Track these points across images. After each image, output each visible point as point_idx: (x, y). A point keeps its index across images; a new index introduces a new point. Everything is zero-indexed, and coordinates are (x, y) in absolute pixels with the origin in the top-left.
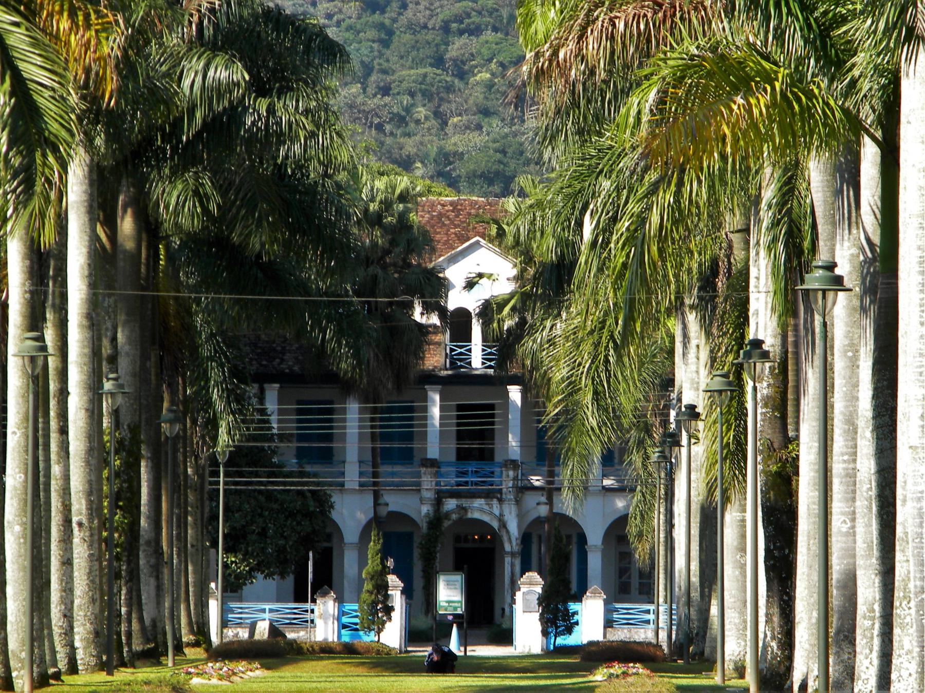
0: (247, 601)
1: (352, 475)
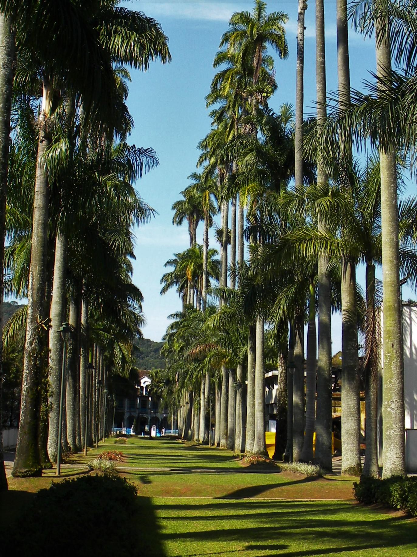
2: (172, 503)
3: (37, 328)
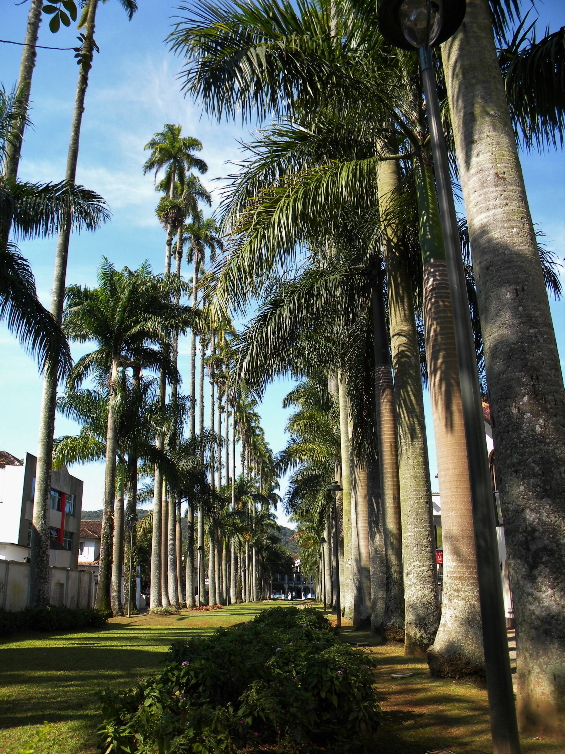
1: (286, 582)
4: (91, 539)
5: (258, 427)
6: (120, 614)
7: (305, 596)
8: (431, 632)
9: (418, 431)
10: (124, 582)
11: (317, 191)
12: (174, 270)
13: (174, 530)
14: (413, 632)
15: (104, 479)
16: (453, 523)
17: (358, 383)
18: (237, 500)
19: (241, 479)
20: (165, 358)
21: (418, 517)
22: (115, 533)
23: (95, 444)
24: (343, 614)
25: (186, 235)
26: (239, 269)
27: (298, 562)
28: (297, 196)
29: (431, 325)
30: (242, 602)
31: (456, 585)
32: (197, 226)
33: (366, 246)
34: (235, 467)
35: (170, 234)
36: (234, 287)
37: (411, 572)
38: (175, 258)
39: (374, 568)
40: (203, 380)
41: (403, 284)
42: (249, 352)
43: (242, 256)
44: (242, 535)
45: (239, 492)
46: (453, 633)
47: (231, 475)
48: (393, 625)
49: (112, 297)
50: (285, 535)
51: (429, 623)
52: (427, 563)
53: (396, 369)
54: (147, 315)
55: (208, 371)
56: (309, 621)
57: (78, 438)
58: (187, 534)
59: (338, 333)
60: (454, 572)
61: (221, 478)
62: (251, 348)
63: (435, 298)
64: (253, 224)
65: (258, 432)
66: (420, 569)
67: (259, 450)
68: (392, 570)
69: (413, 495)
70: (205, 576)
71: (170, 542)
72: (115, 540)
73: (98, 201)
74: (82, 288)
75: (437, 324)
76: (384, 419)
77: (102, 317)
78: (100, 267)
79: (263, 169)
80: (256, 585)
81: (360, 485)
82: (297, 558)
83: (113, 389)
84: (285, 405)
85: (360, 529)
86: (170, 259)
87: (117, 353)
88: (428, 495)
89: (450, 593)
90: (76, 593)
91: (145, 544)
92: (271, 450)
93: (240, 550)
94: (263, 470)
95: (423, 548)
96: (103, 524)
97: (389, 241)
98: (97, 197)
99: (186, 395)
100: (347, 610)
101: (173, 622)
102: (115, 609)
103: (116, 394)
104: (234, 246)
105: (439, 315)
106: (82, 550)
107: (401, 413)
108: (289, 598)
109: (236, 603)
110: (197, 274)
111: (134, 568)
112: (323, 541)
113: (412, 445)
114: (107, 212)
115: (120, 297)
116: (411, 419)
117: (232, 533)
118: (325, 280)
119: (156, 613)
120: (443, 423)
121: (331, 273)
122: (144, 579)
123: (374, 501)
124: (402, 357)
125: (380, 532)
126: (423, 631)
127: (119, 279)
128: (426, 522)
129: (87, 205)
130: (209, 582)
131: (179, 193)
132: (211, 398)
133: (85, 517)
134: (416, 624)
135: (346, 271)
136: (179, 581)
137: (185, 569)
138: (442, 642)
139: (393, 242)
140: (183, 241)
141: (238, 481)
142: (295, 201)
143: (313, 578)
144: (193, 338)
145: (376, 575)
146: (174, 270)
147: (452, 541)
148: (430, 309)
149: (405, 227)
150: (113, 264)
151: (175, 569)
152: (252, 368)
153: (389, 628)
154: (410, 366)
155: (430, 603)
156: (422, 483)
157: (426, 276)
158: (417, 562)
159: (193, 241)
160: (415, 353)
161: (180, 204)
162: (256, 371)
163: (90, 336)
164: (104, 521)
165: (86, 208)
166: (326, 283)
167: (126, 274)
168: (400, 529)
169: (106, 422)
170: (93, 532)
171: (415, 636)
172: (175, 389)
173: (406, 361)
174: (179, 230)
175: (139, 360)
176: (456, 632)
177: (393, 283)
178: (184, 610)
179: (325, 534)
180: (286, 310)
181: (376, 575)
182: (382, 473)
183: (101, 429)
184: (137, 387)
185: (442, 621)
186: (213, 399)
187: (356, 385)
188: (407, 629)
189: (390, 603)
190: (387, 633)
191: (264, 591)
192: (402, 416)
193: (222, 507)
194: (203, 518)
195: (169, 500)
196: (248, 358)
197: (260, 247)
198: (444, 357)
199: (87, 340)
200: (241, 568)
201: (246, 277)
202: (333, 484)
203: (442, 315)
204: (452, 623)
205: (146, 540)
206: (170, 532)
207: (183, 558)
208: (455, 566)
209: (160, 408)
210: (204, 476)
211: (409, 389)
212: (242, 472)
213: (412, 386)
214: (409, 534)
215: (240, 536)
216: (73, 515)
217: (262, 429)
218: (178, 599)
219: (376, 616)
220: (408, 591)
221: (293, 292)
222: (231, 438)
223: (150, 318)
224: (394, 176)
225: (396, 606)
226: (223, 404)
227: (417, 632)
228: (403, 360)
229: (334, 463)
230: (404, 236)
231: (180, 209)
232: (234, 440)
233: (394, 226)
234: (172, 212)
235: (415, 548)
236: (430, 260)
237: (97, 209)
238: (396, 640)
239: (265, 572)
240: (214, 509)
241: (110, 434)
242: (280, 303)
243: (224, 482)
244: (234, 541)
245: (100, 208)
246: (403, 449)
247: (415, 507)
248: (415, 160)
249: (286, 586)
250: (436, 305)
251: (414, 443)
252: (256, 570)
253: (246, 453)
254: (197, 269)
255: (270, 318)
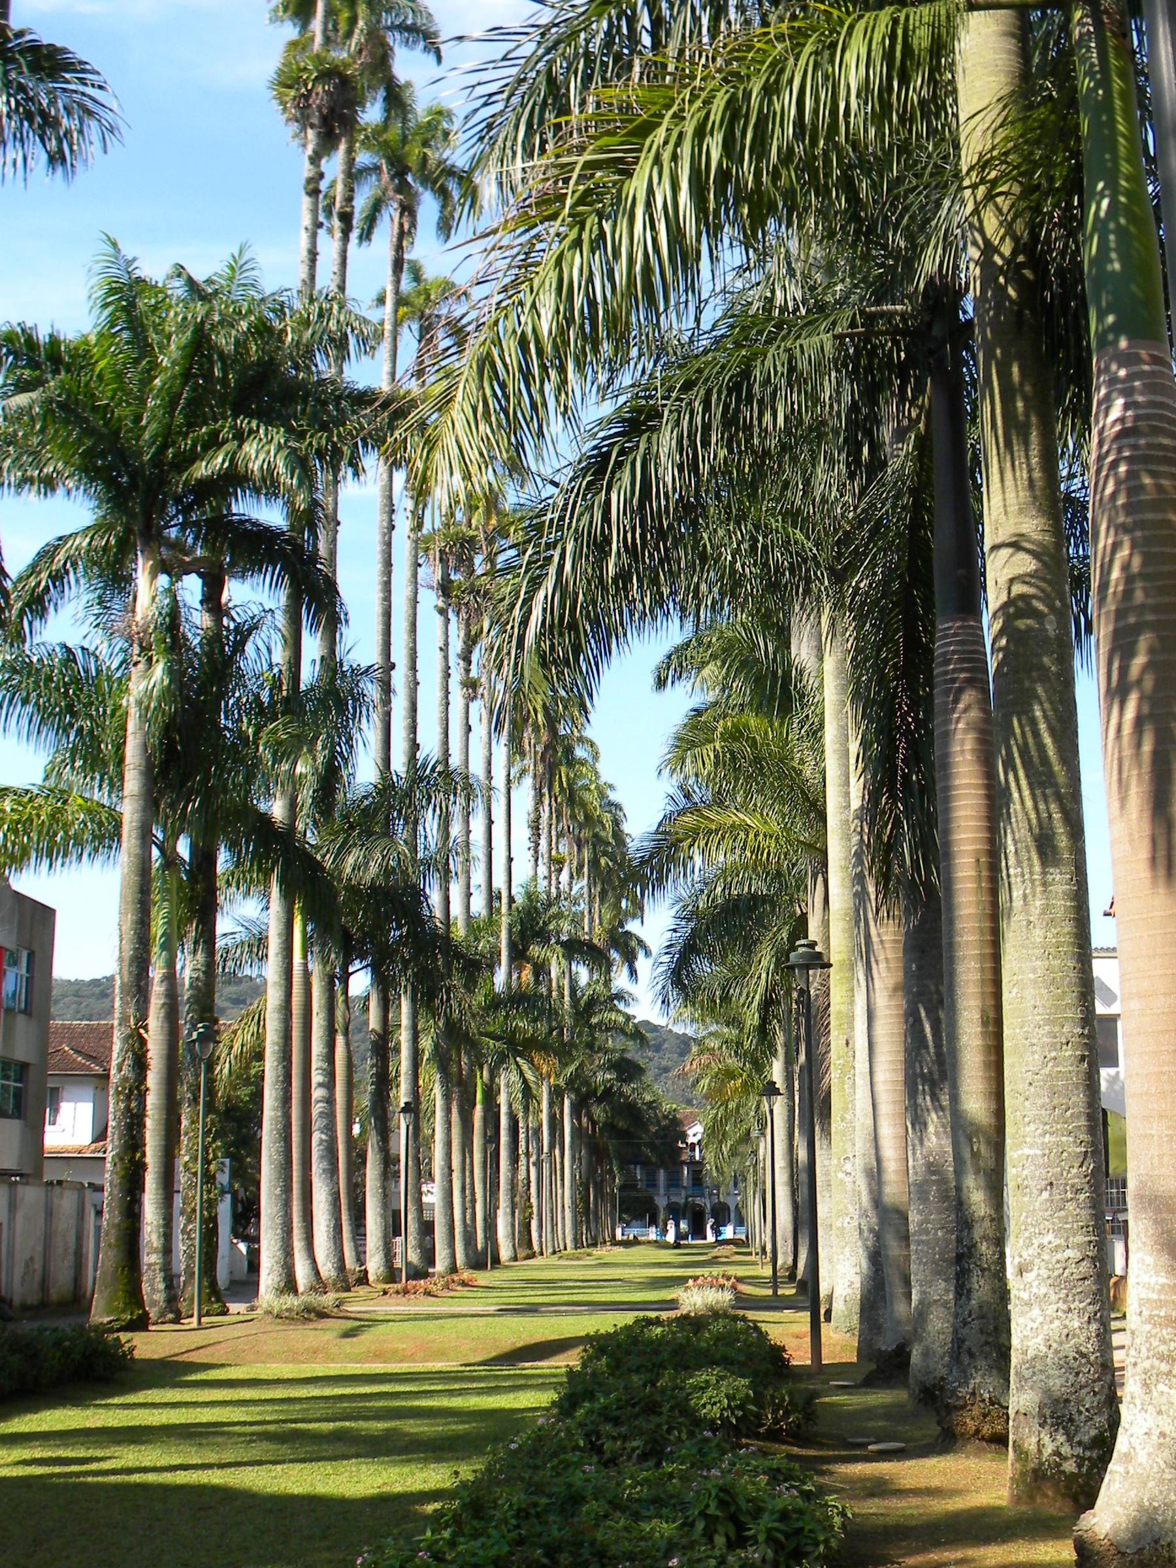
0: (149, 1387)
1: (662, 1191)
2: (309, 1375)
3: (130, 1036)
4: (81, 1078)
5: (581, 740)
6: (171, 1316)
7: (718, 1233)
8: (1086, 1439)
9: (1063, 841)
10: (182, 1221)
11: (770, 103)
12: (326, 280)
13: (330, 1057)
14: (1034, 1440)
15: (115, 918)
16: (1161, 1156)
17: (886, 660)
18: (518, 954)
19: (529, 896)
20: (298, 549)
21: (1056, 1102)
22: (153, 1080)
23: (89, 811)
24: (828, 1313)
25: (364, 158)
26: (523, 344)
27: (695, 1132)
28: (708, 114)
29: (1116, 546)
30: (532, 1256)
31: (1163, 1341)
32: (396, 128)
33: (915, 251)
34: (510, 859)
35: (315, 160)
36: (507, 399)
37: (1032, 1263)
38: (330, 231)
39: (920, 1212)
40: (414, 602)
41: (1028, 388)
42: (552, 570)
43: (534, 305)
44: (531, 1062)
45: (522, 933)
46: (1151, 1484)
47: (499, 882)
48: (973, 1394)
49: (137, 361)
50: (658, 1048)
51: (1080, 1413)
52: (1080, 1239)
53: (1000, 649)
54: (243, 422)
55: (431, 573)
56: (727, 1396)
57: (36, 791)
58: (367, 1069)
59: (824, 500)
60: (1160, 1304)
61: (469, 895)
62: (556, 559)
63: (1130, 460)
64: (569, 202)
65: (580, 752)
66: (1059, 1256)
67: (583, 805)
68: (977, 1233)
69: (1042, 1035)
70: (422, 1173)
71: (317, 1093)
72: (153, 1100)
73: (82, 81)
74: (43, 335)
75: (1133, 546)
76: (960, 874)
77: (106, 425)
78: (97, 268)
79: (600, 15)
80: (574, 1202)
81: (881, 957)
82: (693, 1119)
83: (141, 645)
84: (661, 683)
85: (880, 1088)
86: (314, 237)
87: (152, 536)
88: (1088, 1037)
89: (1147, 1364)
90: (40, 1249)
91: (244, 1093)
92: (618, 807)
93: (526, 1109)
94: (594, 863)
95: (1069, 1195)
96: (115, 1055)
97: (989, 249)
98: (78, 67)
99: (364, 664)
100: (838, 1307)
101: (328, 1342)
102: (154, 1303)
103: (150, 660)
104: (510, 267)
105: (1139, 517)
106: (56, 1111)
107: (1013, 785)
108: (671, 1237)
109: (515, 1259)
110: (397, 282)
111: (209, 1178)
112: (771, 1090)
113: (1045, 884)
114: (109, 116)
115: (158, 365)
116: (1042, 806)
117: (502, 1059)
118: (788, 350)
119: (278, 1316)
120: (1144, 853)
121: (806, 325)
122: (241, 1194)
123: (923, 1014)
124: (1020, 614)
125: (942, 1108)
126: (1061, 1438)
127: (155, 308)
128: (1078, 1118)
129: (48, 93)
130: (433, 1195)
131: (343, 27)
132: (439, 655)
133: (64, 996)
134: (1042, 1415)
135: (853, 325)
136: (344, 1208)
137: (364, 1163)
138: (1118, 1509)
139: (1001, 255)
140: (353, 175)
141: (520, 900)
142: (701, 133)
143: (739, 1179)
144: (385, 476)
145: (927, 1232)
146: (326, 280)
147: (1158, 1211)
148: (1114, 496)
149: (1037, 209)
150: (135, 259)
151: (333, 1171)
152: (562, 617)
153: (961, 1403)
154: (1043, 641)
155: (1083, 1355)
156: (1071, 998)
157: (1103, 391)
158: (1050, 1237)
159: (386, 177)
160: (1058, 603)
161: (346, 65)
162: (573, 626)
163: (71, 484)
164: (117, 1047)
165: (45, 102)
166: (791, 358)
167: (178, 289)
168: (999, 1113)
169: (120, 747)
170: (89, 1057)
171: (1040, 1452)
172: (331, 643)
173: (1030, 629)
174: (343, 147)
175: (221, 552)
176: (1162, 1481)
177: (996, 384)
178: (362, 1291)
179: (776, 1071)
180: (666, 441)
181: (927, 1232)
182: (951, 945)
183: (105, 764)
184: (214, 639)
185: (1122, 1444)
186: (446, 658)
187: (879, 669)
188: (1016, 1428)
189: (964, 1331)
190: (956, 1417)
191: (597, 1218)
192: (1016, 795)
193: (470, 985)
194: (414, 1016)
195: (315, 967)
196: (549, 583)
197: (590, 279)
198: (1151, 651)
199: (60, 491)
200: (528, 1155)
201: (544, 368)
202: (801, 950)
203: (1150, 516)
204: (1149, 1454)
205: (247, 1082)
206: (316, 1063)
207: (356, 1130)
208: (1163, 1286)
209: (287, 700)
210: (418, 895)
211: (1038, 714)
212: (531, 873)
213: (1047, 706)
214: (1027, 1151)
215: (525, 1067)
216: (27, 1012)
217: (592, 745)
218: (342, 1259)
219: (926, 1354)
220: (1021, 1320)
221: (688, 386)
222: (499, 781)
223: (251, 432)
224: (1011, 44)
225: (983, 1338)
226: (474, 674)
227: (1046, 1440)
228: (1022, 624)
229: (805, 864)
230: (1034, 236)
231: (345, 82)
232: (509, 781)
233: (1003, 202)
234: (320, 89)
235: (1046, 1195)
236: (1116, 342)
237: (81, 106)
238: (983, 1439)
239: (600, 1162)
240: (448, 994)
241: (132, 782)
242: (650, 417)
243: (478, 905)
244: (508, 1083)
245: (90, 104)
246: (1015, 894)
247: (1047, 1070)
248: (1078, 14)
249: (661, 1202)
250: (1132, 483)
251: (1050, 878)
252: (573, 1157)
253: (545, 816)
254: (398, 265)
255: (619, 465)
